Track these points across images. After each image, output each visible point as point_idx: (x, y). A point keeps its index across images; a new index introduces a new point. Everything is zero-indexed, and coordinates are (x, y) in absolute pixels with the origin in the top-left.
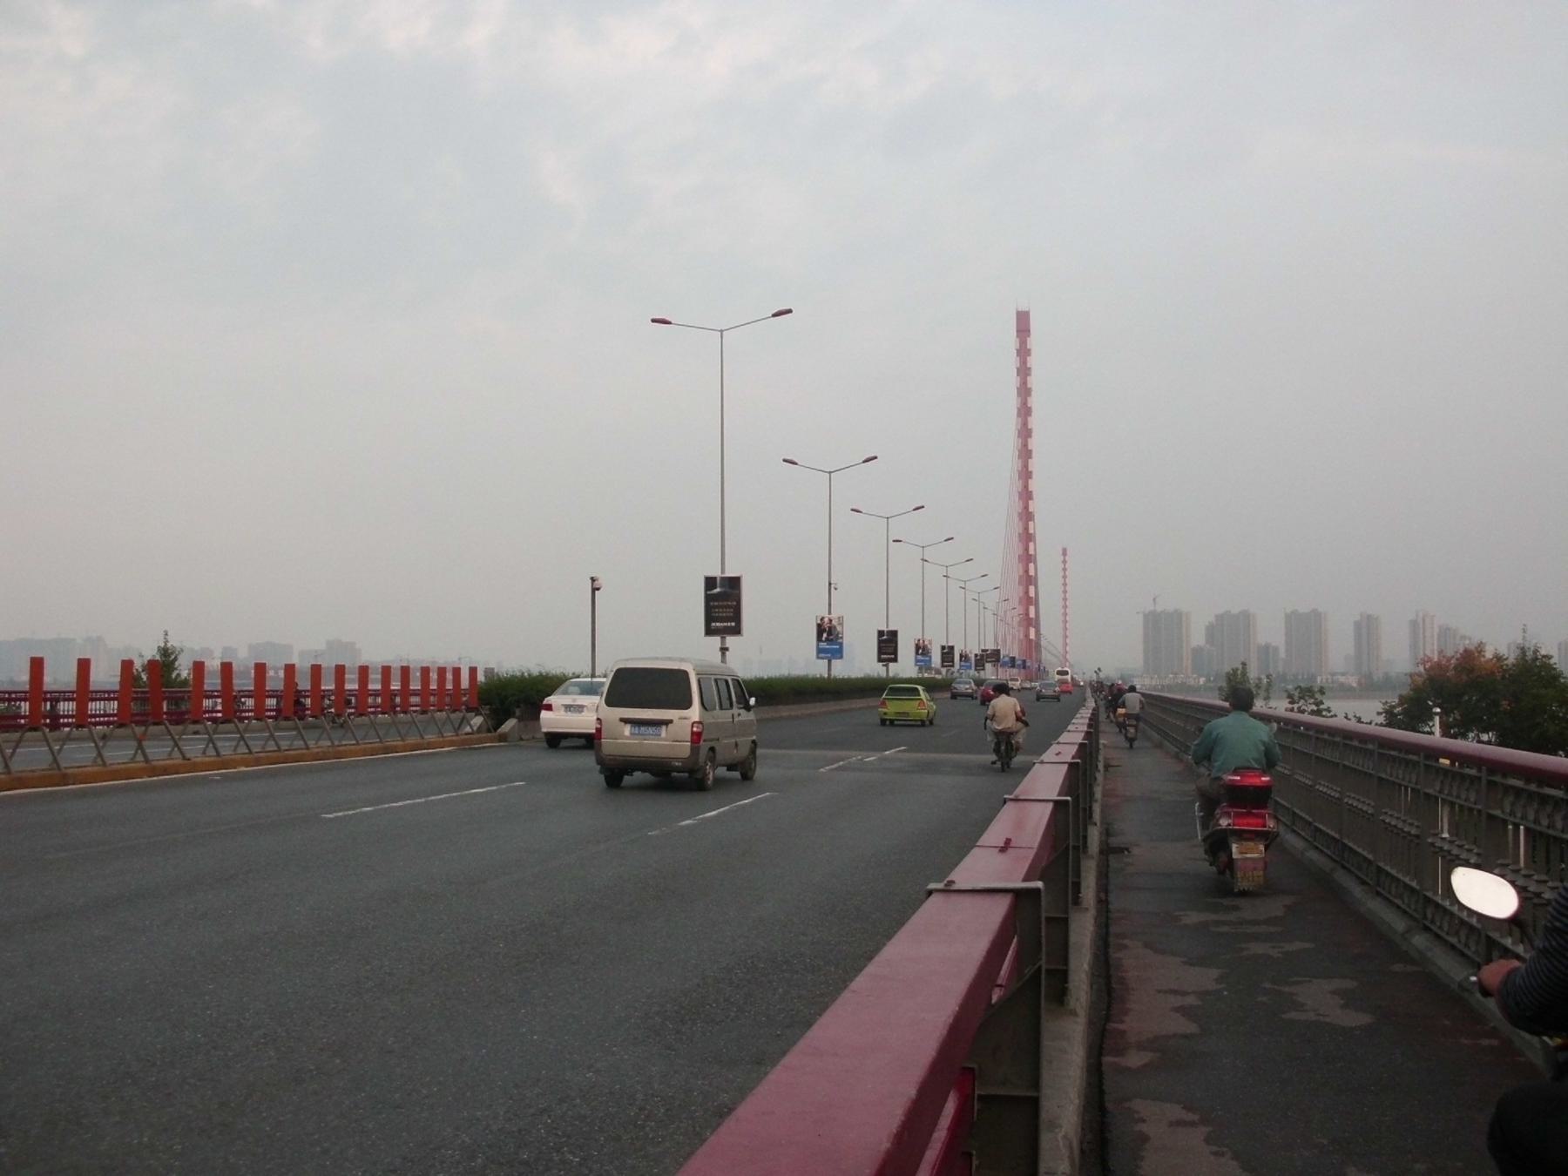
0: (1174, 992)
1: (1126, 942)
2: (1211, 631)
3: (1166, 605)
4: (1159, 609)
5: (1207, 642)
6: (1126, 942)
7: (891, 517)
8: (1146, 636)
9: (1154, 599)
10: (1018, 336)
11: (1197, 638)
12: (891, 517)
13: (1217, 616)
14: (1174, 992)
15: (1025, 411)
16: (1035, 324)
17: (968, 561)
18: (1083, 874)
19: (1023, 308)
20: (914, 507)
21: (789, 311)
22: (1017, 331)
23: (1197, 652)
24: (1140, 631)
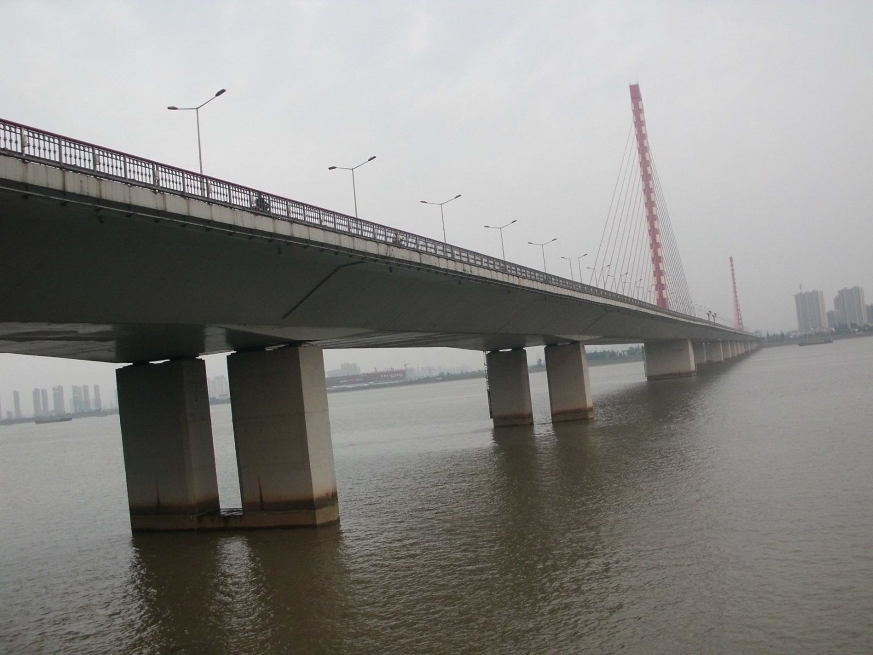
0: (632, 144)
1: (6, 651)
2: (837, 301)
3: (808, 289)
4: (804, 291)
5: (836, 308)
6: (6, 651)
7: (199, 107)
8: (799, 316)
9: (800, 286)
10: (632, 102)
11: (829, 305)
12: (199, 107)
13: (839, 292)
14: (632, 144)
15: (735, 288)
16: (734, 259)
18: (286, 339)
19: (633, 83)
20: (455, 196)
21: (375, 157)
22: (632, 98)
23: (830, 315)
24: (794, 305)
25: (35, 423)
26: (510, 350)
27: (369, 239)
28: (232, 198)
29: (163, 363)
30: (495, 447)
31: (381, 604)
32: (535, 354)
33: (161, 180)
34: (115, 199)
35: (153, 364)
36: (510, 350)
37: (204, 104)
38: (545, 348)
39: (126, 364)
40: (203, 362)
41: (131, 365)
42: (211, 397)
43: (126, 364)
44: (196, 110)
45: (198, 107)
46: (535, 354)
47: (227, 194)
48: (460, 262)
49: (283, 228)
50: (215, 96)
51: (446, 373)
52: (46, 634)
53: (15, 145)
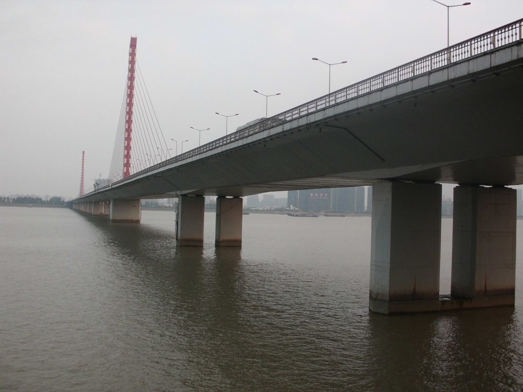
17: (218, 114)
25: (287, 215)
26: (227, 197)
27: (304, 116)
28: (433, 64)
29: (490, 187)
30: (61, 199)
31: (274, 383)
32: (211, 199)
33: (385, 82)
34: (280, 132)
35: (511, 189)
36: (505, 186)
37: (441, 4)
38: (455, 189)
39: (509, 187)
40: (204, 198)
41: (491, 187)
42: (450, 219)
43: (509, 187)
44: (329, 65)
45: (331, 64)
46: (211, 199)
47: (368, 86)
48: (240, 140)
49: (295, 125)
50: (318, 60)
51: (16, 198)
52: (303, 314)
53: (517, 32)
